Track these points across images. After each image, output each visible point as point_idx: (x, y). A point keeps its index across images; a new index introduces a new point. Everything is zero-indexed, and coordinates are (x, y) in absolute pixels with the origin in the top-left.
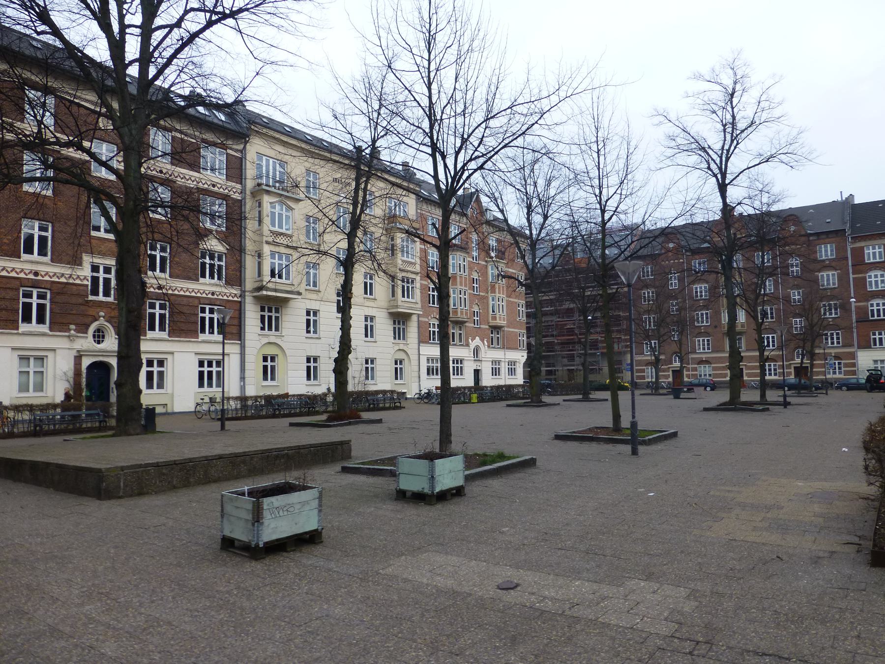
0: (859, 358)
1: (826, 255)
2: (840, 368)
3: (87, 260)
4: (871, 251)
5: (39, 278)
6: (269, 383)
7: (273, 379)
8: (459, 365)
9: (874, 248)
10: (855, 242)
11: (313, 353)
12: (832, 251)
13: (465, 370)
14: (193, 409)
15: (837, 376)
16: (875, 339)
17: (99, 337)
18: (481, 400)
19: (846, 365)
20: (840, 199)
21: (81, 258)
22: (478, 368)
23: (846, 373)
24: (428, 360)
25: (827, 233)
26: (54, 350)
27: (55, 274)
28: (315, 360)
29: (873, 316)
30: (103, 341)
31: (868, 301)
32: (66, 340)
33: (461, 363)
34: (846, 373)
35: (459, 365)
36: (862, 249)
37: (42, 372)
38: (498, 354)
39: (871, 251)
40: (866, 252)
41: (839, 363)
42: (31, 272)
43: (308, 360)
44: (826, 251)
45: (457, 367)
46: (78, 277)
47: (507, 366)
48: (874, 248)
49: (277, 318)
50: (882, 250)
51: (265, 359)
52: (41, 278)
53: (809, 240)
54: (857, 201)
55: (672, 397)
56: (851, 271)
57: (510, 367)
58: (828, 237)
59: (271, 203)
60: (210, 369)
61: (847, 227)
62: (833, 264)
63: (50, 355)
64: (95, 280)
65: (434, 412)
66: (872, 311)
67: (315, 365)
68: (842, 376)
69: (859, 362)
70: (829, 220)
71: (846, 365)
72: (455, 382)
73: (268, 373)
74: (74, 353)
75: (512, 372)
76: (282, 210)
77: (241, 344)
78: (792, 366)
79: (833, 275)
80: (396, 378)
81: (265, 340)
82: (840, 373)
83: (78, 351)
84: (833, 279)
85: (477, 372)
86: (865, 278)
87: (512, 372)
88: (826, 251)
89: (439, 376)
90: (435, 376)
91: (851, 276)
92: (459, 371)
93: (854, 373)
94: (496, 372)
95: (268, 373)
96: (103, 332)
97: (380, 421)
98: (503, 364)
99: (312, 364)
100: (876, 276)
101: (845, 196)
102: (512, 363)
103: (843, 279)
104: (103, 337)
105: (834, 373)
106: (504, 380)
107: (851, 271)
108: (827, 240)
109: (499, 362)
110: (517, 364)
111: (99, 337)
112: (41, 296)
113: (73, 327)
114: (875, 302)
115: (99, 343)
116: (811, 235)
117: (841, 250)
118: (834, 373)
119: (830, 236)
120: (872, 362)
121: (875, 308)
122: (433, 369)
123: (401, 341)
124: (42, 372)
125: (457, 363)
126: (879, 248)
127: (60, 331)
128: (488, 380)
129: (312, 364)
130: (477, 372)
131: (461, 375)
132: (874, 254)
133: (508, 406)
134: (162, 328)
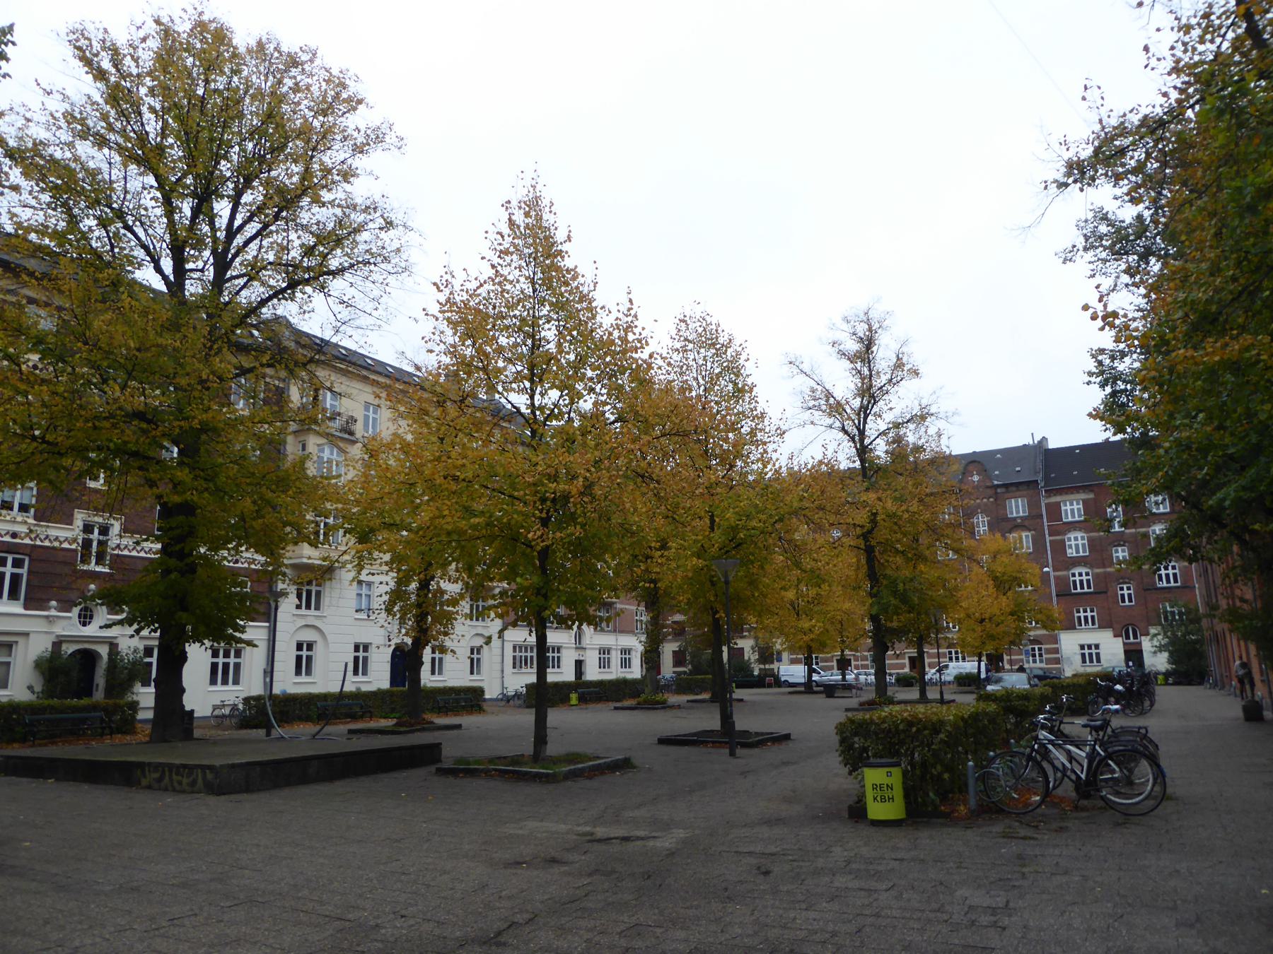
0: (1063, 642)
1: (1018, 512)
2: (1041, 655)
3: (80, 517)
4: (1069, 507)
5: (17, 541)
6: (303, 678)
7: (365, 673)
8: (606, 656)
9: (1072, 504)
10: (1050, 496)
11: (363, 639)
12: (1023, 506)
13: (564, 662)
14: (209, 714)
15: (1038, 665)
16: (1079, 618)
17: (85, 617)
18: (583, 699)
19: (1049, 651)
20: (1031, 443)
21: (72, 515)
22: (581, 658)
23: (1049, 661)
24: (514, 648)
25: (1018, 485)
26: (26, 634)
27: (66, 539)
28: (366, 648)
29: (1075, 588)
30: (90, 623)
31: (1068, 569)
32: (43, 621)
33: (558, 652)
34: (1049, 661)
35: (606, 656)
36: (1058, 505)
37: (8, 664)
38: (607, 640)
39: (1069, 507)
40: (1063, 508)
41: (1040, 649)
42: (7, 533)
43: (357, 648)
44: (1017, 507)
45: (526, 657)
46: (47, 537)
47: (620, 656)
48: (1072, 504)
49: (318, 594)
50: (1081, 506)
51: (299, 647)
52: (20, 541)
53: (996, 493)
54: (1053, 444)
55: (824, 695)
56: (1047, 532)
57: (602, 656)
58: (1018, 490)
59: (318, 445)
60: (226, 660)
61: (1039, 478)
62: (1026, 523)
63: (21, 640)
64: (87, 544)
65: (527, 718)
66: (1074, 582)
67: (365, 654)
68: (1043, 665)
69: (1063, 647)
70: (1018, 469)
71: (1049, 651)
72: (552, 677)
73: (303, 665)
74: (52, 638)
75: (626, 663)
76: (332, 454)
77: (269, 627)
78: (907, 656)
79: (1027, 536)
80: (472, 673)
81: (303, 622)
82: (1041, 661)
83: (58, 636)
84: (1028, 542)
85: (579, 664)
86: (1063, 542)
87: (626, 663)
88: (1017, 507)
89: (535, 670)
90: (529, 670)
91: (1048, 539)
92: (558, 663)
93: (1057, 661)
94: (604, 663)
95: (303, 665)
96: (91, 611)
97: (459, 727)
98: (613, 653)
99: (361, 654)
100: (1076, 539)
101: (1037, 439)
102: (626, 651)
103: (1038, 542)
104: (91, 617)
105: (1035, 661)
106: (615, 672)
107: (1047, 532)
108: (1018, 493)
109: (630, 651)
110: (633, 653)
111: (85, 617)
112: (17, 563)
113: (54, 603)
114: (1076, 571)
115: (84, 624)
116: (998, 486)
117: (1033, 505)
118: (1035, 661)
119: (1020, 488)
120: (1078, 648)
121: (1077, 578)
122: (526, 664)
123: (312, 612)
124: (8, 664)
125: (526, 651)
126: (1078, 504)
127: (37, 610)
128: (593, 673)
129: (304, 653)
130: (579, 664)
131: (558, 667)
132: (1072, 511)
133: (616, 708)
134: (13, 595)
